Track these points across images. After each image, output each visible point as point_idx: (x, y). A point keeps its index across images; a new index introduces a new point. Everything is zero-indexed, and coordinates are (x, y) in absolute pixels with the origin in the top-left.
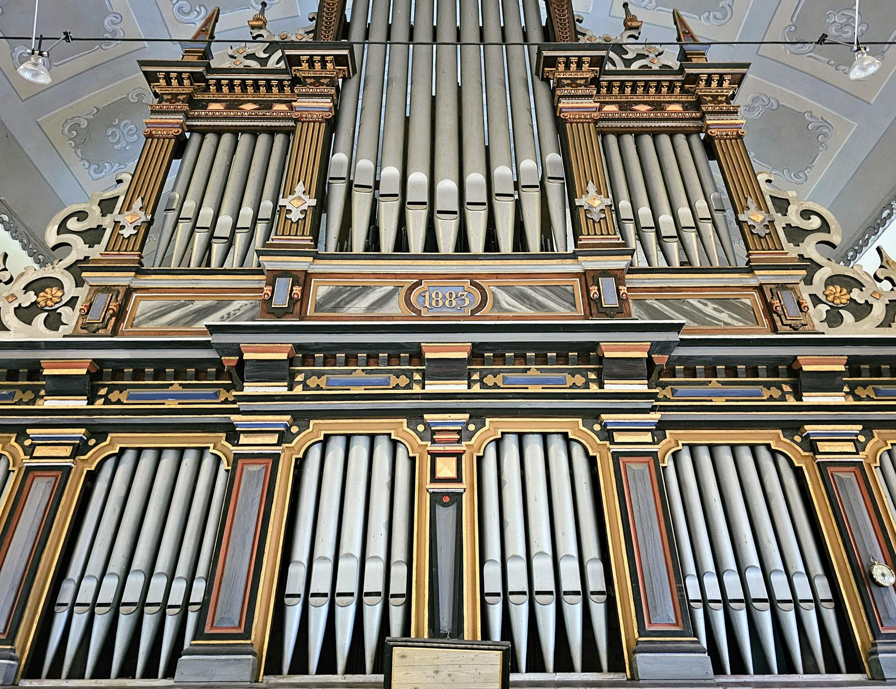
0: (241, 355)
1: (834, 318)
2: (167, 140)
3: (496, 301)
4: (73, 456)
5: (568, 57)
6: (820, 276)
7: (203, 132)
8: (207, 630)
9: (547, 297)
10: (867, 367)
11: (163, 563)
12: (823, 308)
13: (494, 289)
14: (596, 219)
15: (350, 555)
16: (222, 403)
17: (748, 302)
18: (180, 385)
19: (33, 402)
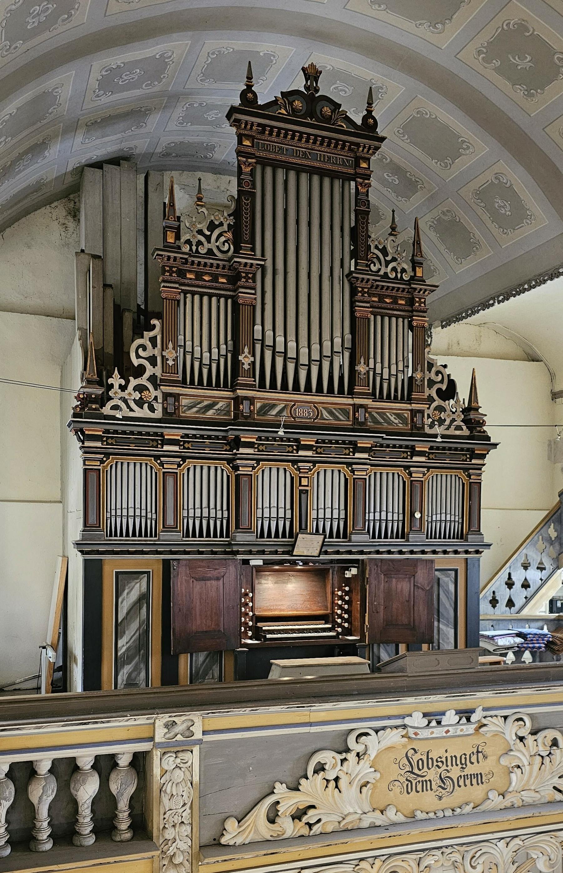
1: (431, 426)
6: (434, 405)
11: (205, 504)
12: (430, 420)
14: (362, 377)
15: (274, 507)
17: (406, 415)
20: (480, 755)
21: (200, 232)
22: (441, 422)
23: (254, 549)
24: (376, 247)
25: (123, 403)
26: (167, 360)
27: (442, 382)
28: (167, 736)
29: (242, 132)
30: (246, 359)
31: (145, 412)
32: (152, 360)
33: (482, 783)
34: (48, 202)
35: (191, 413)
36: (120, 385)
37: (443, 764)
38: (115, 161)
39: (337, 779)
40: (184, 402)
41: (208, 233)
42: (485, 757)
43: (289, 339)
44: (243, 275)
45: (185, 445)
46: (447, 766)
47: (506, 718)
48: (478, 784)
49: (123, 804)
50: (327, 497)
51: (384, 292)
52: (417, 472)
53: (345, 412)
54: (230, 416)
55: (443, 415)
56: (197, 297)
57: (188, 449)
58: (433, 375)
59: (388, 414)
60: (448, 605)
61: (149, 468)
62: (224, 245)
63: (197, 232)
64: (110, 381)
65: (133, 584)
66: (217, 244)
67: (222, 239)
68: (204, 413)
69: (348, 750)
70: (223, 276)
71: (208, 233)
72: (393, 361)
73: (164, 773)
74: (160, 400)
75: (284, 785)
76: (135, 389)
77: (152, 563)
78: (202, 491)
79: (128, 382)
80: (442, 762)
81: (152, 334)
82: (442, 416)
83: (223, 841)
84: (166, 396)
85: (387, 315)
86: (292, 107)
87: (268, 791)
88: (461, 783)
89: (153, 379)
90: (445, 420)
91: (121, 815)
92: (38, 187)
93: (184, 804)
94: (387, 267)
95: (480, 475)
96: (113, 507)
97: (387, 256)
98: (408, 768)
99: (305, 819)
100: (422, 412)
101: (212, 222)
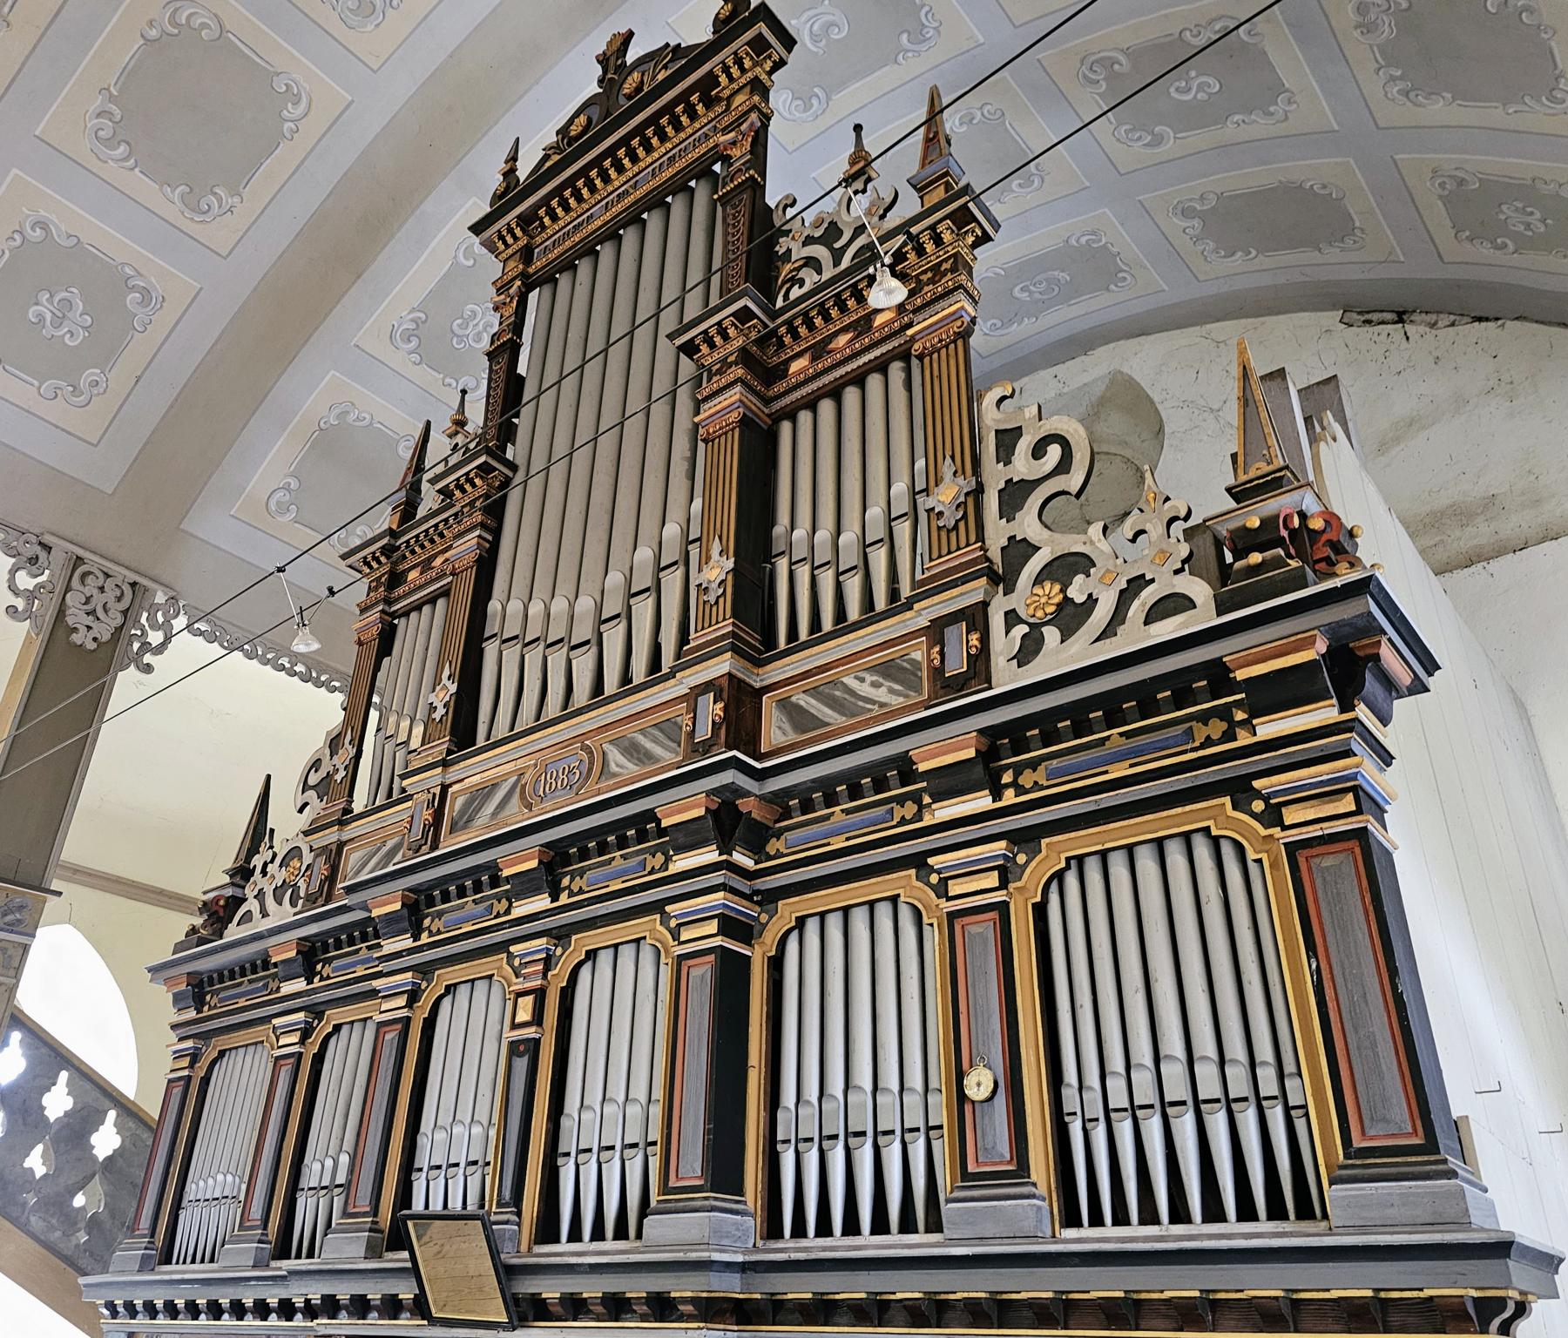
0: (659, 822)
2: (935, 356)
4: (1003, 884)
5: (705, 332)
7: (791, 415)
8: (672, 1183)
9: (656, 741)
10: (1036, 732)
16: (1202, 747)
18: (1121, 734)
19: (918, 817)
22: (1070, 616)
23: (682, 1288)
27: (1064, 466)
45: (1021, 781)
61: (905, 915)
82: (1071, 593)
90: (1092, 601)
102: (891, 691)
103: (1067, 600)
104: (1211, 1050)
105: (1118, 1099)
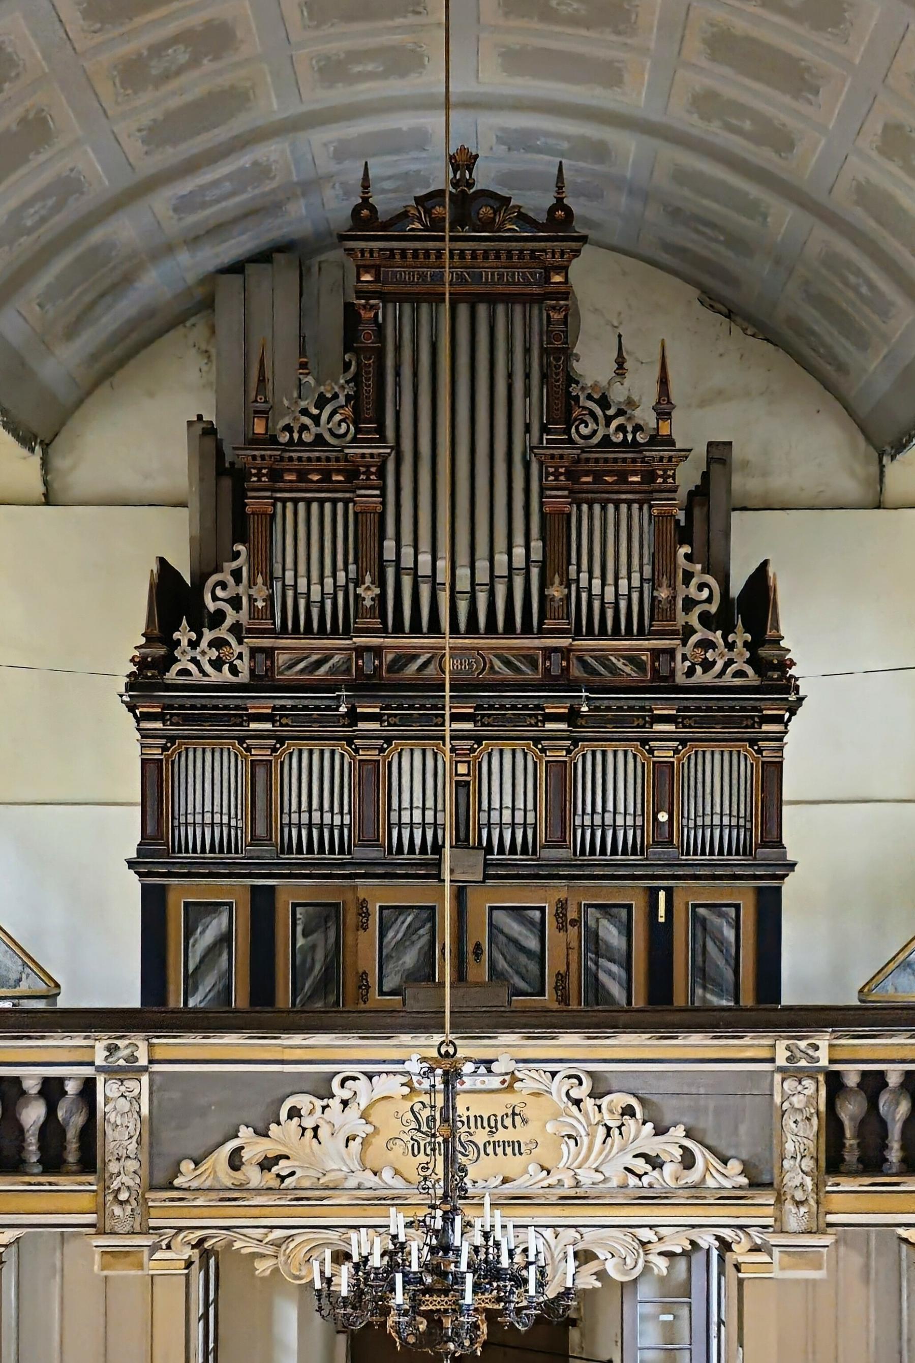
1: (691, 672)
3: (492, 667)
6: (694, 639)
11: (315, 805)
13: (491, 657)
14: (556, 605)
17: (644, 658)
20: (517, 1118)
21: (305, 412)
24: (589, 397)
25: (193, 666)
26: (256, 600)
27: (709, 600)
28: (110, 1060)
29: (360, 263)
30: (369, 593)
31: (226, 675)
32: (235, 603)
33: (521, 1154)
34: (179, 320)
35: (290, 675)
36: (190, 641)
37: (463, 1125)
38: (264, 257)
39: (316, 1129)
40: (282, 659)
41: (315, 412)
42: (525, 1121)
43: (439, 555)
44: (362, 469)
46: (469, 1128)
47: (554, 1074)
48: (514, 1154)
49: (72, 1134)
50: (510, 789)
51: (601, 466)
52: (660, 749)
53: (532, 662)
54: (350, 674)
55: (710, 655)
56: (301, 506)
57: (287, 725)
58: (692, 591)
59: (612, 658)
60: (721, 962)
62: (339, 425)
63: (300, 412)
64: (176, 635)
65: (209, 919)
66: (330, 426)
67: (338, 417)
68: (311, 673)
69: (332, 1096)
70: (339, 472)
71: (315, 412)
72: (623, 572)
73: (107, 1100)
74: (246, 658)
75: (251, 1129)
76: (211, 644)
77: (235, 890)
78: (314, 787)
79: (200, 636)
80: (462, 1122)
81: (235, 565)
82: (708, 655)
83: (176, 1182)
84: (254, 651)
85: (609, 501)
86: (430, 217)
87: (232, 1132)
88: (490, 1150)
89: (236, 629)
90: (714, 663)
91: (69, 1147)
92: (149, 314)
93: (131, 1137)
94: (608, 425)
95: (781, 749)
96: (183, 811)
97: (609, 408)
98: (414, 1125)
99: (275, 1169)
100: (671, 652)
101: (321, 395)
102: (632, 669)
103: (706, 658)
104: (719, 811)
105: (699, 822)
